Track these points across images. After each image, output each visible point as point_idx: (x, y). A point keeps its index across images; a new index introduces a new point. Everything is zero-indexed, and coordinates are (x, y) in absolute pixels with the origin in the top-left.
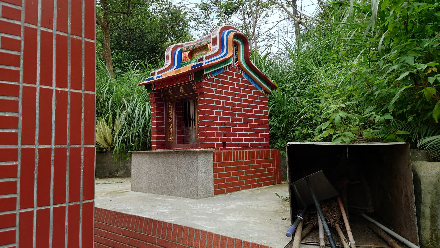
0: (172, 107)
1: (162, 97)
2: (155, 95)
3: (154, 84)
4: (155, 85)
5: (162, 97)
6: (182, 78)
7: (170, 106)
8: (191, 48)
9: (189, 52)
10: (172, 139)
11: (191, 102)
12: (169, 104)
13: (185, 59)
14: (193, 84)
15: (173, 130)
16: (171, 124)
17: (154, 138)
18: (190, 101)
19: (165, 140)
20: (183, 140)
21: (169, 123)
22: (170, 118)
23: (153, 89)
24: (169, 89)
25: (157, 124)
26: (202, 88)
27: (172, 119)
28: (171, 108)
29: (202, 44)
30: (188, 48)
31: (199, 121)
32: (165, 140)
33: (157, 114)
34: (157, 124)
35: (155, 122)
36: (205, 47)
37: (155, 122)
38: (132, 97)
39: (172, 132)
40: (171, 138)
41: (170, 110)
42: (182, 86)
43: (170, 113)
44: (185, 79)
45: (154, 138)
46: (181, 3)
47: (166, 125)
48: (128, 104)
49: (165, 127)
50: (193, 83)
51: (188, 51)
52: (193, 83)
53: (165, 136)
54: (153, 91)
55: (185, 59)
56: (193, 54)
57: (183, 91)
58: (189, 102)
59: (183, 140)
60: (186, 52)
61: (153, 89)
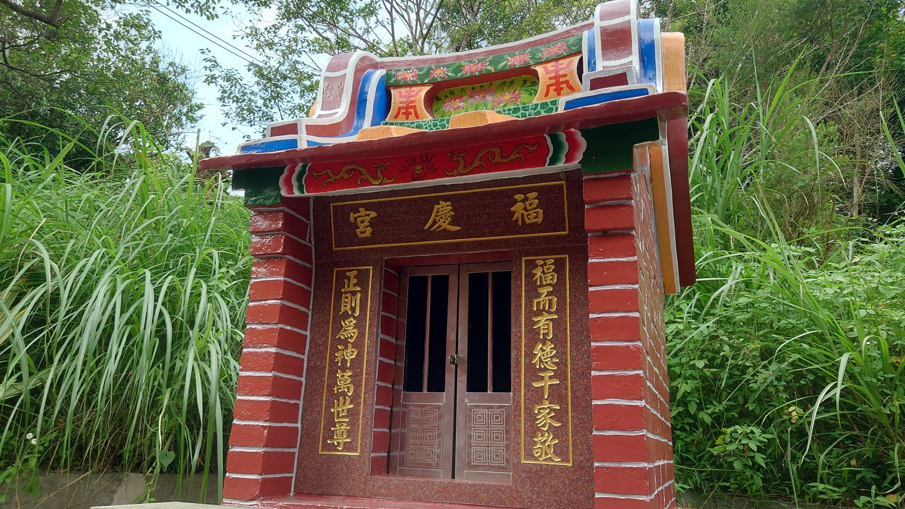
0: (364, 292)
1: (310, 241)
2: (292, 226)
3: (298, 169)
5: (310, 241)
6: (497, 151)
7: (352, 285)
8: (440, 74)
10: (348, 447)
11: (452, 281)
12: (342, 277)
13: (407, 115)
15: (355, 399)
16: (344, 369)
17: (249, 435)
18: (445, 279)
19: (296, 450)
20: (389, 453)
21: (333, 363)
22: (345, 343)
24: (363, 205)
25: (280, 363)
26: (622, 206)
27: (358, 345)
28: (354, 293)
29: (501, 65)
30: (428, 73)
31: (594, 373)
32: (296, 450)
33: (286, 315)
34: (280, 363)
35: (273, 350)
37: (273, 350)
39: (352, 414)
40: (341, 437)
41: (351, 303)
42: (446, 199)
43: (346, 316)
45: (249, 435)
46: (206, 50)
47: (315, 371)
48: (56, 266)
49: (303, 379)
50: (519, 191)
51: (424, 85)
53: (299, 425)
54: (285, 201)
55: (407, 115)
56: (438, 99)
57: (445, 224)
60: (415, 89)
61: (290, 189)
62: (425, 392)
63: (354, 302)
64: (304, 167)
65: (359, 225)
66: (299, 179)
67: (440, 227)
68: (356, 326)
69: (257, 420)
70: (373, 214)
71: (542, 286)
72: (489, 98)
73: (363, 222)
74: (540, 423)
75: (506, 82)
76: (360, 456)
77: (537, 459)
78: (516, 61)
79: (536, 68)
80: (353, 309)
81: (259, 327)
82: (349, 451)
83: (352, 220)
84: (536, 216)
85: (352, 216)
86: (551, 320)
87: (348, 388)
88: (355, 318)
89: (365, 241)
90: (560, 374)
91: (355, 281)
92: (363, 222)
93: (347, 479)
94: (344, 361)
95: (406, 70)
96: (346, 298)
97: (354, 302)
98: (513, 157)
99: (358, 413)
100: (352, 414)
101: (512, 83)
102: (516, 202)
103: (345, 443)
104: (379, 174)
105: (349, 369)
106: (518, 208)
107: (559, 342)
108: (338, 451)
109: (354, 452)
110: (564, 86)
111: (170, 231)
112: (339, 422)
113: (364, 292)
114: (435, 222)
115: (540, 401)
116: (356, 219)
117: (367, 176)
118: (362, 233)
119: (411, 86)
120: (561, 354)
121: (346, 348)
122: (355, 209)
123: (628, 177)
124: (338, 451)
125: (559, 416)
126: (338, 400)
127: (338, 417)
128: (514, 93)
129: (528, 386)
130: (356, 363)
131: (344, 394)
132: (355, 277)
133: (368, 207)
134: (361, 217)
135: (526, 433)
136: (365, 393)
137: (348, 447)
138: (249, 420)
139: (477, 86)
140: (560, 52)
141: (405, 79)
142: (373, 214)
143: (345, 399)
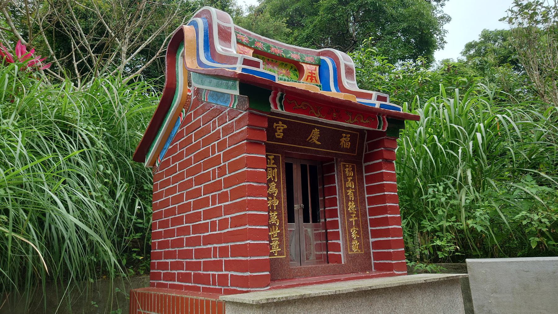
27: (278, 197)
42: (318, 128)
52: (344, 132)
57: (315, 140)
62: (311, 223)
63: (273, 174)
64: (282, 95)
65: (278, 131)
66: (280, 101)
67: (313, 141)
68: (276, 187)
69: (264, 240)
70: (285, 126)
71: (348, 177)
72: (276, 68)
73: (279, 129)
74: (353, 236)
75: (283, 64)
76: (286, 258)
77: (353, 252)
78: (295, 56)
79: (302, 64)
80: (274, 177)
81: (255, 184)
82: (280, 255)
83: (274, 127)
84: (348, 145)
85: (275, 124)
86: (353, 192)
87: (276, 221)
88: (275, 182)
89: (279, 140)
90: (357, 216)
91: (273, 161)
92: (279, 129)
93: (281, 270)
94: (272, 206)
95: (241, 35)
96: (270, 170)
97: (273, 174)
98: (367, 121)
99: (282, 235)
100: (280, 236)
101: (286, 65)
102: (342, 137)
103: (278, 251)
104: (318, 112)
105: (275, 210)
106: (343, 140)
107: (355, 201)
108: (275, 256)
109: (283, 256)
110: (314, 78)
111: (118, 94)
112: (274, 240)
113: (278, 168)
114: (311, 138)
115: (352, 227)
116: (276, 127)
117: (313, 111)
118: (278, 135)
119: (244, 45)
120: (357, 207)
121: (273, 199)
122: (277, 121)
123: (395, 140)
124: (275, 256)
125: (358, 233)
126: (272, 228)
127: (273, 237)
128: (287, 71)
129: (348, 220)
130: (279, 207)
131: (275, 225)
132: (273, 159)
133: (284, 122)
134: (279, 126)
135: (349, 241)
136: (285, 224)
137: (280, 253)
138: (259, 240)
139: (270, 59)
140: (312, 61)
141: (242, 40)
142: (285, 126)
143: (275, 227)
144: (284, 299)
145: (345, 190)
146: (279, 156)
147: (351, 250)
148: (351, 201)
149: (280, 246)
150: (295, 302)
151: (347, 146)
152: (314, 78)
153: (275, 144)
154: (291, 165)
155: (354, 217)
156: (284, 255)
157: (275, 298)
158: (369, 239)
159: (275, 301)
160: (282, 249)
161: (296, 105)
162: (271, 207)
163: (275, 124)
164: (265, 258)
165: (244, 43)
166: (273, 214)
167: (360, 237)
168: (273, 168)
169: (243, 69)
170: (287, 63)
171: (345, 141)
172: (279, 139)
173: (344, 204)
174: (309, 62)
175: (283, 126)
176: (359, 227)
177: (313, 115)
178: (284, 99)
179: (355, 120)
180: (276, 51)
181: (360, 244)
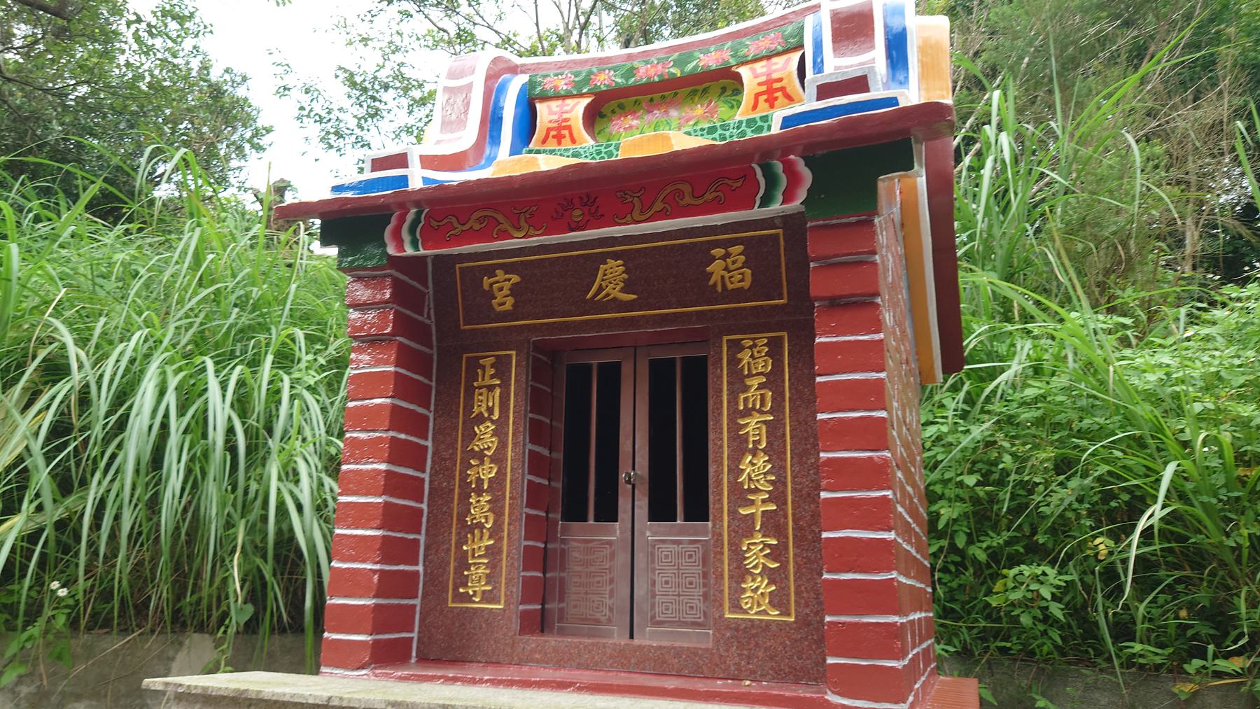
0: (505, 386)
4: (416, 222)
5: (429, 317)
6: (686, 188)
8: (604, 80)
9: (586, 101)
10: (487, 597)
11: (627, 370)
12: (474, 366)
13: (559, 138)
14: (719, 252)
15: (495, 532)
16: (479, 491)
19: (417, 602)
20: (543, 604)
21: (464, 484)
22: (480, 456)
23: (400, 246)
27: (498, 459)
29: (690, 67)
31: (824, 495)
33: (398, 419)
34: (392, 484)
35: (383, 467)
36: (701, 88)
37: (383, 467)
38: (103, 320)
39: (493, 552)
40: (477, 584)
41: (487, 402)
42: (615, 256)
43: (480, 419)
44: (709, 196)
47: (440, 495)
49: (424, 506)
50: (717, 244)
51: (581, 95)
52: (717, 244)
53: (420, 568)
54: (394, 262)
55: (559, 138)
56: (602, 116)
57: (615, 291)
58: (611, 376)
59: (543, 609)
62: (591, 522)
64: (419, 214)
66: (412, 231)
67: (608, 295)
69: (364, 561)
70: (515, 279)
71: (750, 375)
72: (674, 113)
73: (501, 289)
74: (750, 563)
75: (697, 91)
76: (504, 610)
77: (745, 612)
78: (710, 60)
80: (490, 410)
83: (486, 287)
84: (742, 278)
85: (486, 281)
86: (764, 422)
87: (486, 518)
88: (493, 422)
89: (505, 316)
91: (493, 371)
92: (501, 289)
96: (481, 394)
99: (500, 551)
100: (493, 553)
101: (705, 91)
102: (714, 259)
103: (484, 592)
104: (523, 223)
105: (486, 491)
106: (716, 268)
108: (474, 602)
112: (475, 564)
113: (505, 386)
114: (600, 289)
115: (750, 532)
116: (491, 285)
117: (506, 226)
118: (500, 305)
120: (778, 469)
121: (482, 463)
123: (870, 223)
125: (776, 553)
126: (473, 534)
127: (473, 557)
129: (733, 513)
130: (496, 483)
133: (508, 269)
134: (498, 282)
135: (731, 577)
137: (487, 597)
139: (657, 96)
142: (515, 279)
143: (482, 533)
144: (199, 691)
145: (732, 420)
146: (467, 358)
147: (736, 607)
148: (754, 453)
149: (490, 579)
150: (250, 705)
151: (742, 280)
152: (566, 132)
153: (497, 328)
154: (617, 366)
155: (764, 501)
156: (498, 602)
157: (180, 685)
158: (425, 570)
159: (180, 690)
160: (494, 588)
161: (456, 225)
162: (477, 483)
163: (486, 281)
164: (361, 602)
165: (563, 93)
166: (478, 501)
167: (784, 566)
168: (491, 388)
169: (425, 180)
170: (707, 85)
171: (726, 269)
172: (506, 312)
173: (721, 464)
174: (764, 53)
175: (509, 280)
176: (779, 531)
177: (506, 235)
178: (423, 223)
179: (658, 206)
180: (652, 72)
181: (780, 589)
